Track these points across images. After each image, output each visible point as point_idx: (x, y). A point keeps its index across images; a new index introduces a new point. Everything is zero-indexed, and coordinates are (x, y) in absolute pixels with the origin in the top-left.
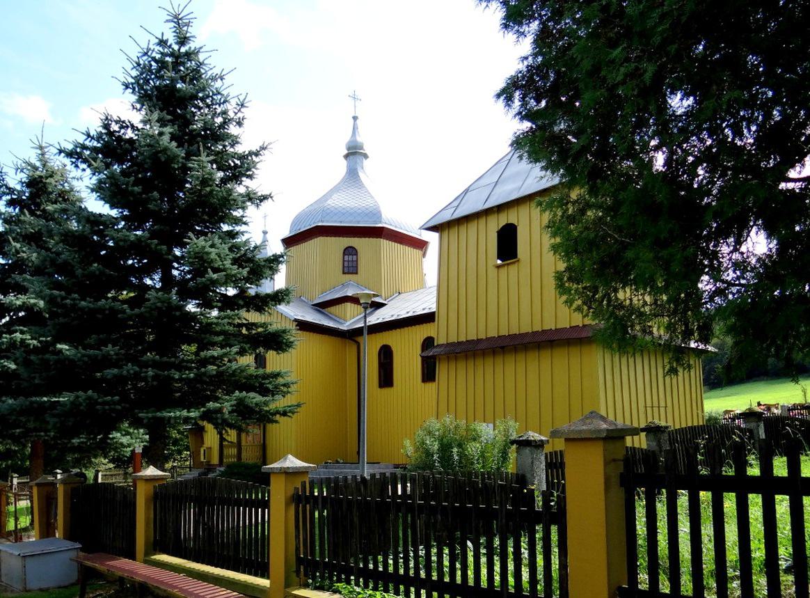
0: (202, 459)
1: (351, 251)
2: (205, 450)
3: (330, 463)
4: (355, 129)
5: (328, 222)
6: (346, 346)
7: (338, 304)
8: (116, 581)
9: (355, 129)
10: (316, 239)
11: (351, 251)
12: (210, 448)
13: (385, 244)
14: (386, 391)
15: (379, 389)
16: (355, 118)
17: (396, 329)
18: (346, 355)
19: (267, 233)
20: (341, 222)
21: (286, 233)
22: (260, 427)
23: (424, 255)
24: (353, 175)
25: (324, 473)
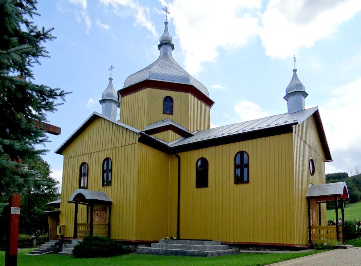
0: (58, 233)
1: (168, 100)
2: (60, 227)
3: (168, 239)
4: (166, 29)
5: (153, 78)
6: (168, 158)
7: (162, 131)
8: (12, 57)
9: (166, 29)
10: (144, 90)
11: (168, 100)
12: (65, 226)
13: (191, 98)
14: (202, 190)
15: (235, 185)
16: (111, 79)
17: (211, 146)
18: (168, 164)
19: (112, 80)
20: (162, 80)
21: (121, 87)
22: (306, 245)
23: (210, 108)
24: (165, 56)
25: (167, 246)
